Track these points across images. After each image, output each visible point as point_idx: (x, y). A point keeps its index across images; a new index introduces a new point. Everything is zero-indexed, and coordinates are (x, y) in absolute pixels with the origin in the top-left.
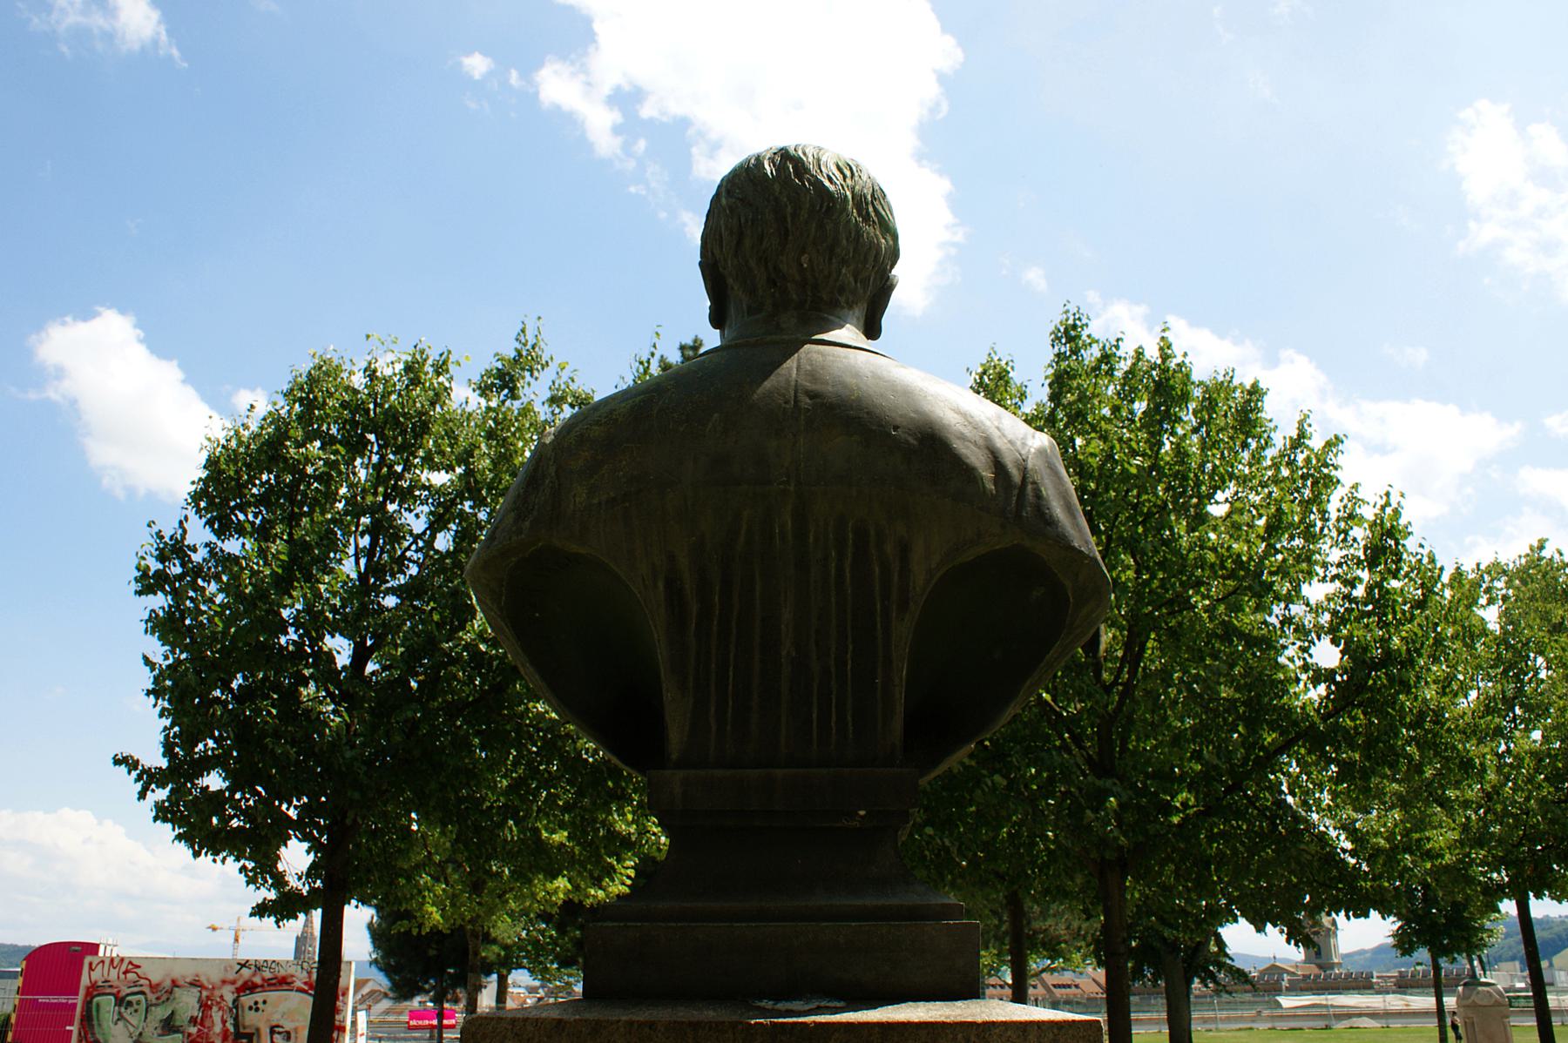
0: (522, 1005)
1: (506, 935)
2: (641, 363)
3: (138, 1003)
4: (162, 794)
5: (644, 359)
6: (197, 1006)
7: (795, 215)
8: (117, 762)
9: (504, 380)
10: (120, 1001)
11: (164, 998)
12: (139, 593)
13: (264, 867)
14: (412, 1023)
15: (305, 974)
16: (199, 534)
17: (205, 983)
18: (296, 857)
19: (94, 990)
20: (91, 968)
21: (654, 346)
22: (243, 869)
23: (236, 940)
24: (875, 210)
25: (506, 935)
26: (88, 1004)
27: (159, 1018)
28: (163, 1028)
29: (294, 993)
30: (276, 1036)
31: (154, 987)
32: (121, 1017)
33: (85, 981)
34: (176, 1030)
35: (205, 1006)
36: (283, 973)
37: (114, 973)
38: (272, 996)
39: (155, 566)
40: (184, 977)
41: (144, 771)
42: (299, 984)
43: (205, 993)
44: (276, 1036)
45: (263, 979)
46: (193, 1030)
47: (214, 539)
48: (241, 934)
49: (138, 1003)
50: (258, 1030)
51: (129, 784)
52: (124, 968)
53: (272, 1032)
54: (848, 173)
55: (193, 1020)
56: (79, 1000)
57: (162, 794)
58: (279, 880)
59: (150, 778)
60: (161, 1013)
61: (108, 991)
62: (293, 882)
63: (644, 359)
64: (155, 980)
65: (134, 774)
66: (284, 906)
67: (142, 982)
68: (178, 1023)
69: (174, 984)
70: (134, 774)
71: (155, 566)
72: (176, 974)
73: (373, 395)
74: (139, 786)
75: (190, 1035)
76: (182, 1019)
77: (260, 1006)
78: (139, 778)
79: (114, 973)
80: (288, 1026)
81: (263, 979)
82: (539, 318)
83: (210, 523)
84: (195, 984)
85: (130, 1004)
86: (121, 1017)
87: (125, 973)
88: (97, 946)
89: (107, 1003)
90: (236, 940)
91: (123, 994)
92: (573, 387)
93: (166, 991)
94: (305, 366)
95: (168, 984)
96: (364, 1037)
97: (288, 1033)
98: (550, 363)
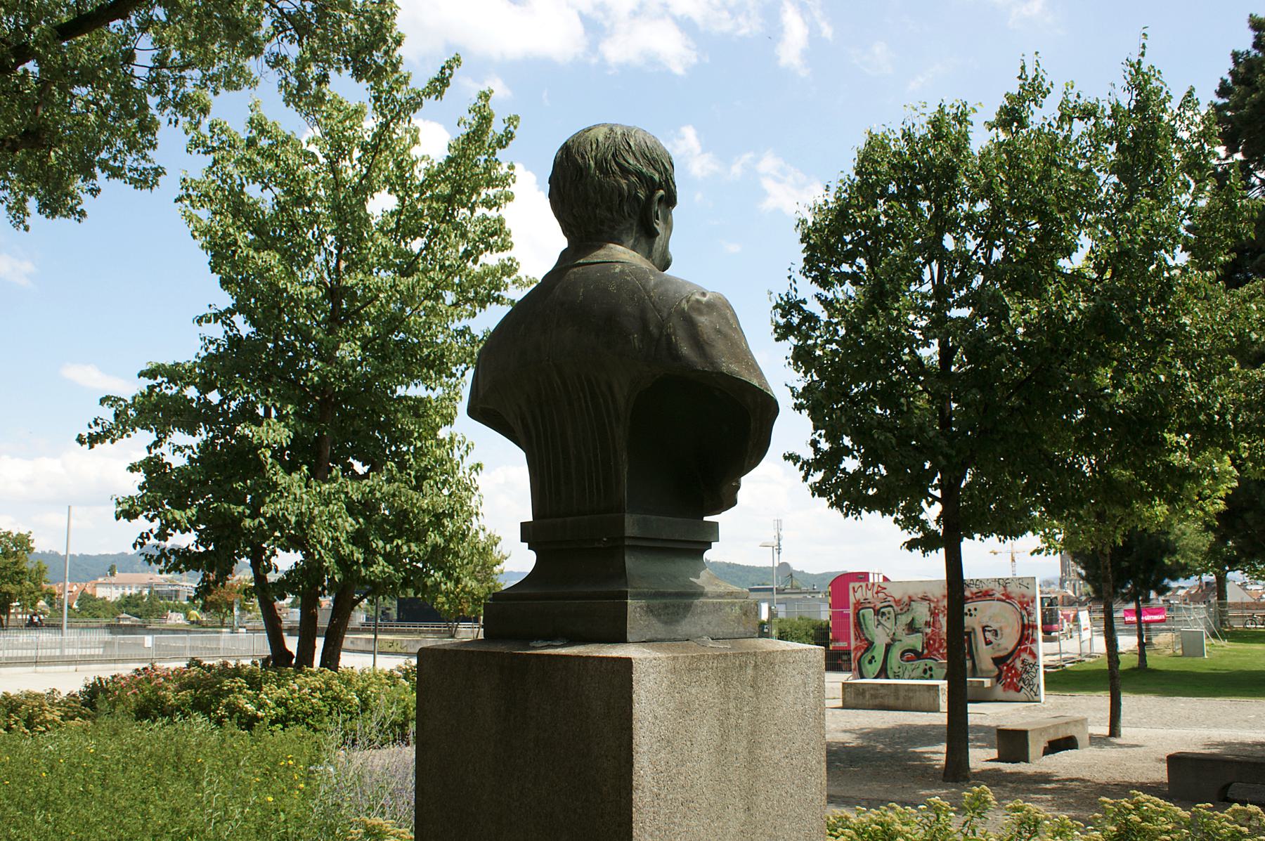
0: (1259, 599)
1: (1201, 544)
2: (1132, 66)
3: (889, 613)
4: (818, 476)
5: (1135, 61)
6: (929, 614)
7: (564, 186)
8: (786, 458)
9: (1011, 117)
10: (877, 612)
11: (905, 609)
12: (777, 340)
13: (911, 520)
14: (1127, 619)
15: (1002, 587)
16: (808, 291)
17: (932, 598)
18: (932, 513)
19: (859, 606)
20: (854, 591)
21: (1144, 47)
22: (896, 521)
23: (1013, 560)
24: (618, 164)
25: (1201, 544)
26: (857, 615)
27: (904, 622)
28: (908, 629)
29: (995, 602)
30: (987, 633)
31: (898, 602)
32: (880, 623)
33: (852, 600)
34: (918, 631)
35: (934, 614)
36: (985, 588)
37: (870, 594)
38: (979, 605)
39: (782, 321)
40: (916, 594)
41: (804, 463)
42: (998, 595)
43: (932, 605)
44: (987, 633)
45: (972, 593)
46: (929, 631)
47: (821, 291)
48: (1015, 555)
49: (889, 613)
50: (974, 629)
51: (796, 472)
52: (875, 590)
53: (984, 631)
54: (594, 146)
55: (927, 624)
56: (851, 611)
57: (818, 476)
58: (923, 525)
59: (808, 467)
60: (904, 619)
61: (868, 605)
62: (933, 526)
63: (1135, 61)
64: (897, 598)
65: (799, 465)
66: (927, 543)
67: (889, 599)
68: (917, 626)
69: (911, 599)
70: (799, 465)
71: (782, 321)
72: (911, 592)
73: (914, 154)
74: (803, 473)
75: (927, 634)
76: (920, 622)
77: (973, 612)
78: (801, 468)
79: (870, 594)
80: (995, 626)
81: (972, 593)
82: (1037, 53)
83: (815, 279)
84: (924, 598)
85: (883, 614)
86: (880, 623)
87: (877, 593)
88: (866, 574)
89: (869, 613)
90: (1013, 560)
91: (878, 607)
92: (1081, 101)
93: (906, 605)
94: (861, 143)
95: (906, 599)
96: (1089, 631)
97: (996, 631)
98: (1051, 89)
